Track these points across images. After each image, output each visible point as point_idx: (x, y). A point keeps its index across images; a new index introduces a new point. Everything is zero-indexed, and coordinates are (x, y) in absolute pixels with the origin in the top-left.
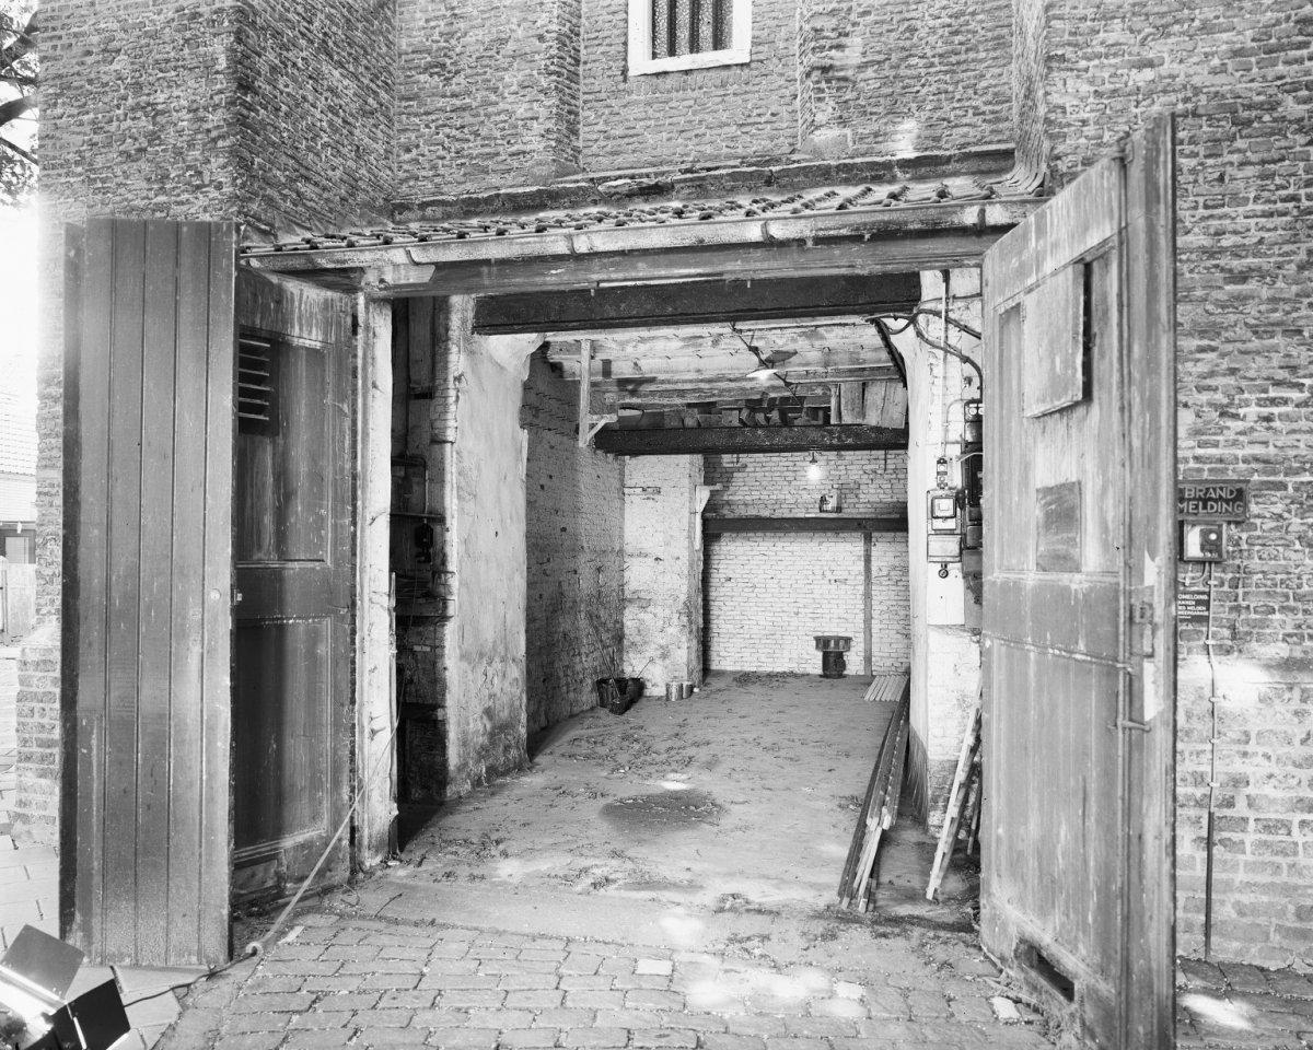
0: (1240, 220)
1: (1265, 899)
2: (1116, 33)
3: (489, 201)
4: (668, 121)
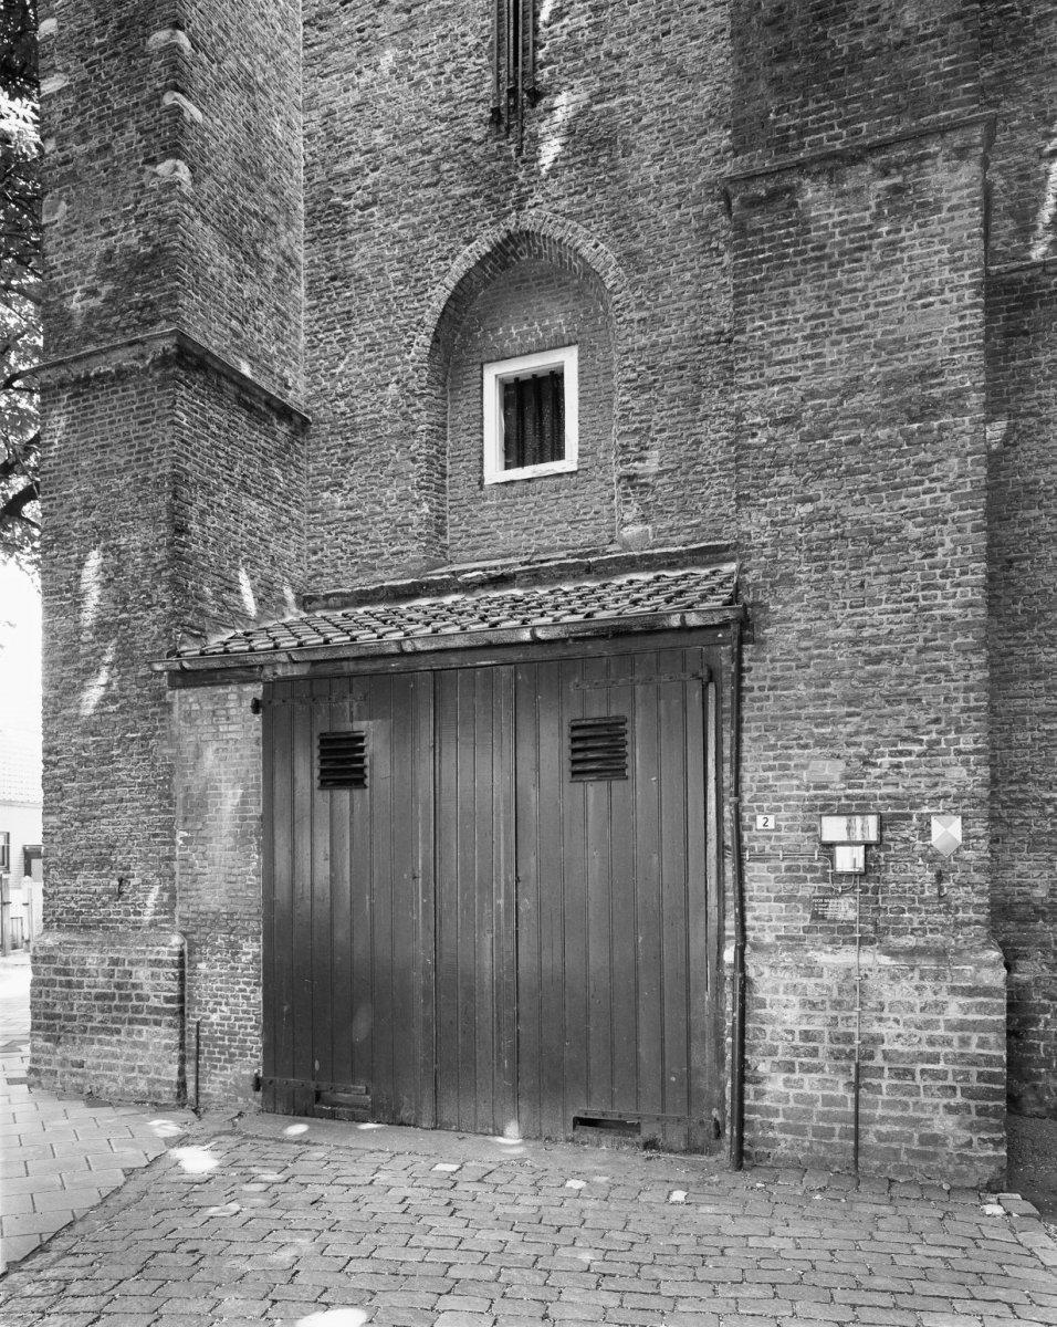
0: (876, 616)
1: (897, 1129)
2: (785, 478)
3: (375, 592)
4: (515, 521)
